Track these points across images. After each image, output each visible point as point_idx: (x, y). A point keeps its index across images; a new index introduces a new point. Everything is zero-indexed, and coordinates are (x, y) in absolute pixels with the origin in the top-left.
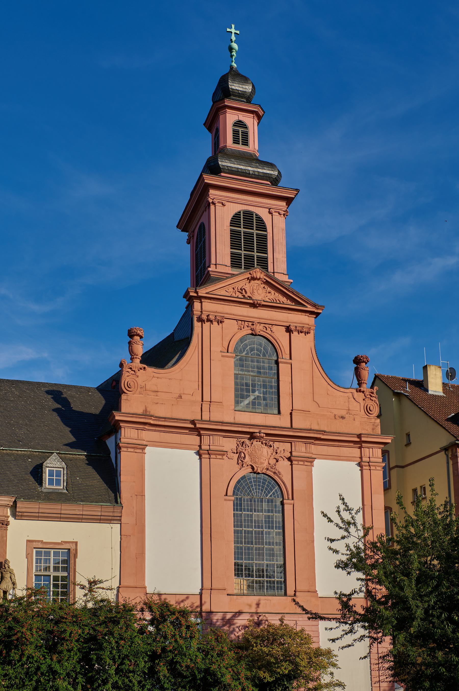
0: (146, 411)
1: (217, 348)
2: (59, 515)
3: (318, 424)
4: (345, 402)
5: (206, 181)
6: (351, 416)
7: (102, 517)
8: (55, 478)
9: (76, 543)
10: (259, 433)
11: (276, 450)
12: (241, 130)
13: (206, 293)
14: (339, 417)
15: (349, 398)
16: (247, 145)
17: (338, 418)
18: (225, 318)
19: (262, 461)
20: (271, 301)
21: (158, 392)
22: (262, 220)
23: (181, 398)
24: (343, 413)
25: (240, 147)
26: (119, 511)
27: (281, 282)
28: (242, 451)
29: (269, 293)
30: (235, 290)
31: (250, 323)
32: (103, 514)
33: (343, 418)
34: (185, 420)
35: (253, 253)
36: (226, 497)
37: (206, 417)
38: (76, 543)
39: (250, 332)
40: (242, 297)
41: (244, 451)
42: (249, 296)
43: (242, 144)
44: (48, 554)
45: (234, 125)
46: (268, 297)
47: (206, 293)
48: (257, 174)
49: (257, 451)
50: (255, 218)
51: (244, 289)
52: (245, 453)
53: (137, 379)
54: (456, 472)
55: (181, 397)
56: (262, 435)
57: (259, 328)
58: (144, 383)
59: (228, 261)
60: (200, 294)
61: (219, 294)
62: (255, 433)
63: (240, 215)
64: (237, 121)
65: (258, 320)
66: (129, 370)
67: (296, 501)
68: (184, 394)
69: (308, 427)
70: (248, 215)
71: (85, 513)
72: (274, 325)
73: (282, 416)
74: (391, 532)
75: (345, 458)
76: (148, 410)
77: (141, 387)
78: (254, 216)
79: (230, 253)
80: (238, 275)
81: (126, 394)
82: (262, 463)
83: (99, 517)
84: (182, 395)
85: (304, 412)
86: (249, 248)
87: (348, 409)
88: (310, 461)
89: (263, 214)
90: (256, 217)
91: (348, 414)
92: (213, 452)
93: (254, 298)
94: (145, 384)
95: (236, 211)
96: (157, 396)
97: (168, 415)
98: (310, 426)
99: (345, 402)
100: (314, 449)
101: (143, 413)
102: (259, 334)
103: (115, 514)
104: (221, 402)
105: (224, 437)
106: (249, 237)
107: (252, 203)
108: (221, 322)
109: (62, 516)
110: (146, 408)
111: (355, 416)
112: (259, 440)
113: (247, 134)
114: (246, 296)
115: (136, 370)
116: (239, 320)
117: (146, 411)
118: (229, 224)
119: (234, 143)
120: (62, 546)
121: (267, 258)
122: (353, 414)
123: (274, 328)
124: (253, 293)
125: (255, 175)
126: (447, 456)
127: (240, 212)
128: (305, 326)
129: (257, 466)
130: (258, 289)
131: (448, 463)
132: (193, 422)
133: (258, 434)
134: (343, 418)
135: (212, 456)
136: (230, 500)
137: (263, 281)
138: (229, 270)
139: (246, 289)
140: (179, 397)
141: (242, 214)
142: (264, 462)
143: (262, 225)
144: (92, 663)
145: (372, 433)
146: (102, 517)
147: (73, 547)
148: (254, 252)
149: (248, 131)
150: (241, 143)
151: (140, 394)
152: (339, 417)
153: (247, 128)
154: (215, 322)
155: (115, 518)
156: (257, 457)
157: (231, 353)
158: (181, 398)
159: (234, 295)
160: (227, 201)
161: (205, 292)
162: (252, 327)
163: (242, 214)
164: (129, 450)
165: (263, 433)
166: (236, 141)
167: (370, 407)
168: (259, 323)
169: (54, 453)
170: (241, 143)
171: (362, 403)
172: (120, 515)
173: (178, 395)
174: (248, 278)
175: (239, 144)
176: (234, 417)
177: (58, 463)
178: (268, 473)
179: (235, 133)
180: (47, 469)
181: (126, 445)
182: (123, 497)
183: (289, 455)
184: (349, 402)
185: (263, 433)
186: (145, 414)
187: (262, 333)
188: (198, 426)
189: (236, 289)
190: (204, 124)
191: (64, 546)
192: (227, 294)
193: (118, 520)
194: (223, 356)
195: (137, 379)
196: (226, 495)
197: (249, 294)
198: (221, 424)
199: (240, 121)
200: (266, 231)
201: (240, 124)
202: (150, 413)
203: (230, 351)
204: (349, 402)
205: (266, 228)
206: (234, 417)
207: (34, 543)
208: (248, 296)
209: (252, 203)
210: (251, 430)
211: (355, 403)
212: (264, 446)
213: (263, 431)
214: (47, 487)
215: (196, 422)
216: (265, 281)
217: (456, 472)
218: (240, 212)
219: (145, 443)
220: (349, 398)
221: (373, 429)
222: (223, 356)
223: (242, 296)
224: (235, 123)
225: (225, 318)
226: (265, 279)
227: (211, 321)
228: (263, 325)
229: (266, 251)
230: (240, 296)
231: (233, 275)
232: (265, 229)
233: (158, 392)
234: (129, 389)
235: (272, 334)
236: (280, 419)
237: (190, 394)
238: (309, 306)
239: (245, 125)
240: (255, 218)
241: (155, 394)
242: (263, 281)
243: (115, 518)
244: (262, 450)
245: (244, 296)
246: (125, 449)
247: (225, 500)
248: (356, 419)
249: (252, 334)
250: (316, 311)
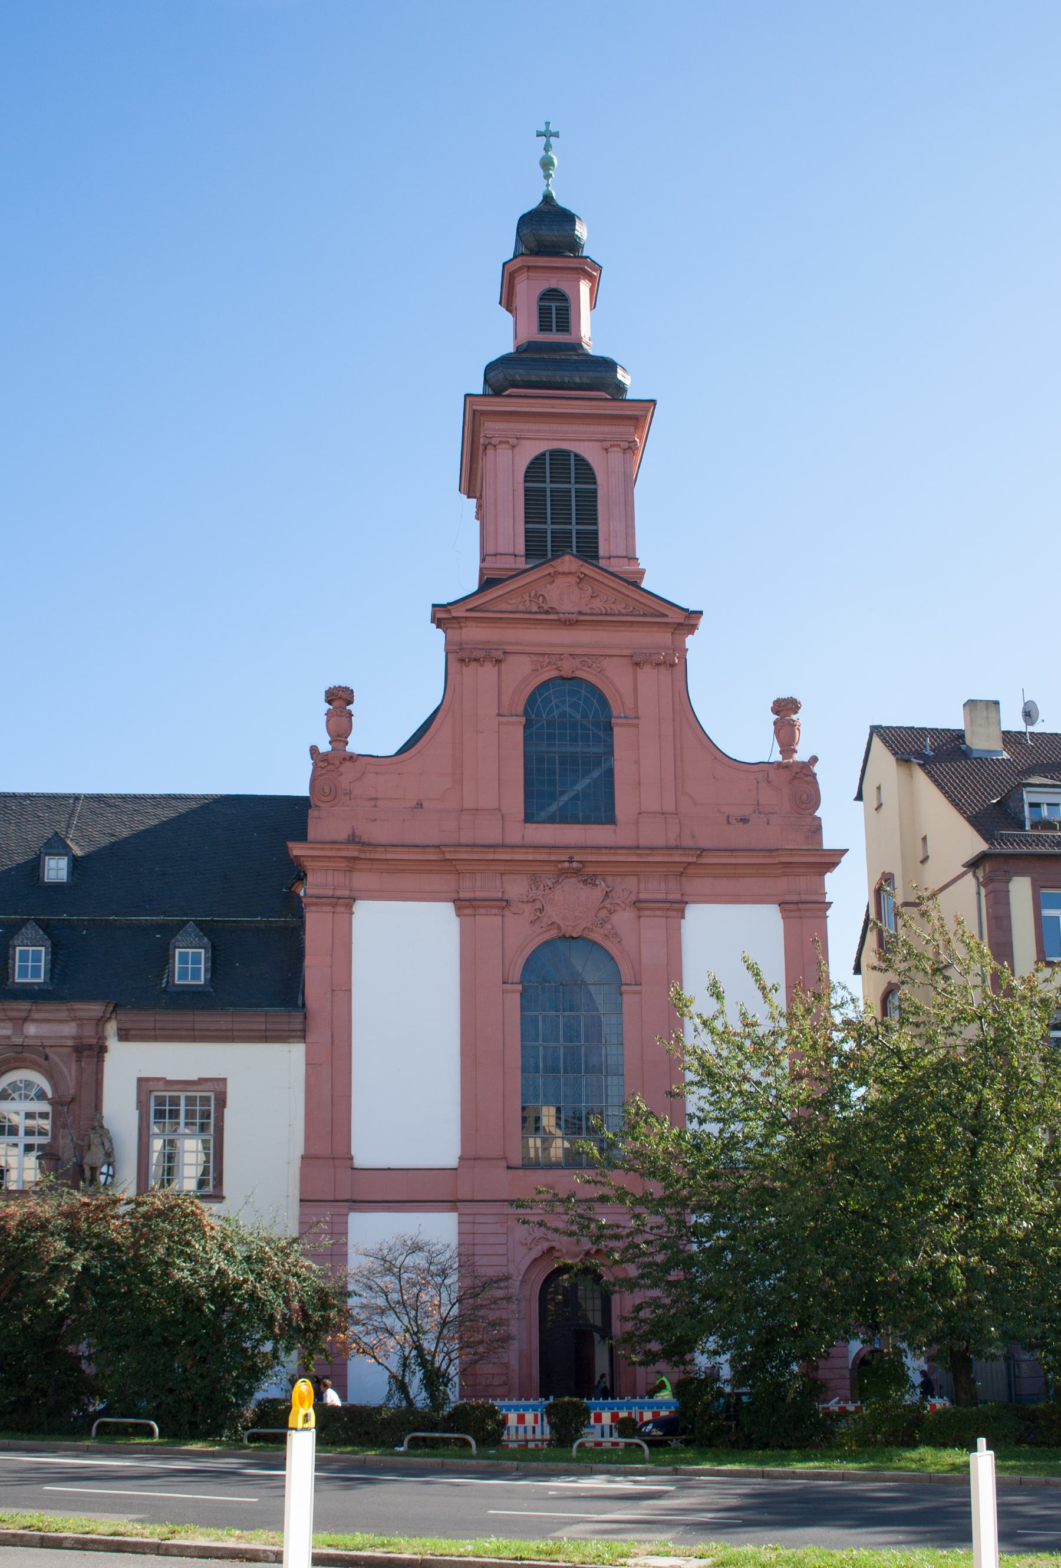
8: (190, 966)
12: (554, 305)
13: (468, 610)
17: (735, 822)
21: (377, 799)
22: (588, 464)
24: (746, 811)
32: (269, 1026)
33: (744, 820)
35: (568, 527)
43: (557, 330)
45: (541, 299)
47: (468, 610)
51: (541, 595)
74: (224, 1507)
76: (357, 833)
78: (572, 458)
90: (575, 460)
96: (375, 806)
110: (353, 830)
123: (605, 663)
126: (978, 879)
131: (979, 893)
134: (744, 820)
136: (513, 992)
139: (546, 595)
141: (548, 457)
144: (83, 1394)
150: (554, 328)
163: (548, 457)
169: (188, 921)
175: (551, 330)
193: (302, 1035)
200: (595, 483)
205: (595, 478)
207: (151, 1083)
213: (576, 858)
220: (758, 782)
221: (814, 833)
236: (615, 832)
239: (564, 296)
241: (373, 803)
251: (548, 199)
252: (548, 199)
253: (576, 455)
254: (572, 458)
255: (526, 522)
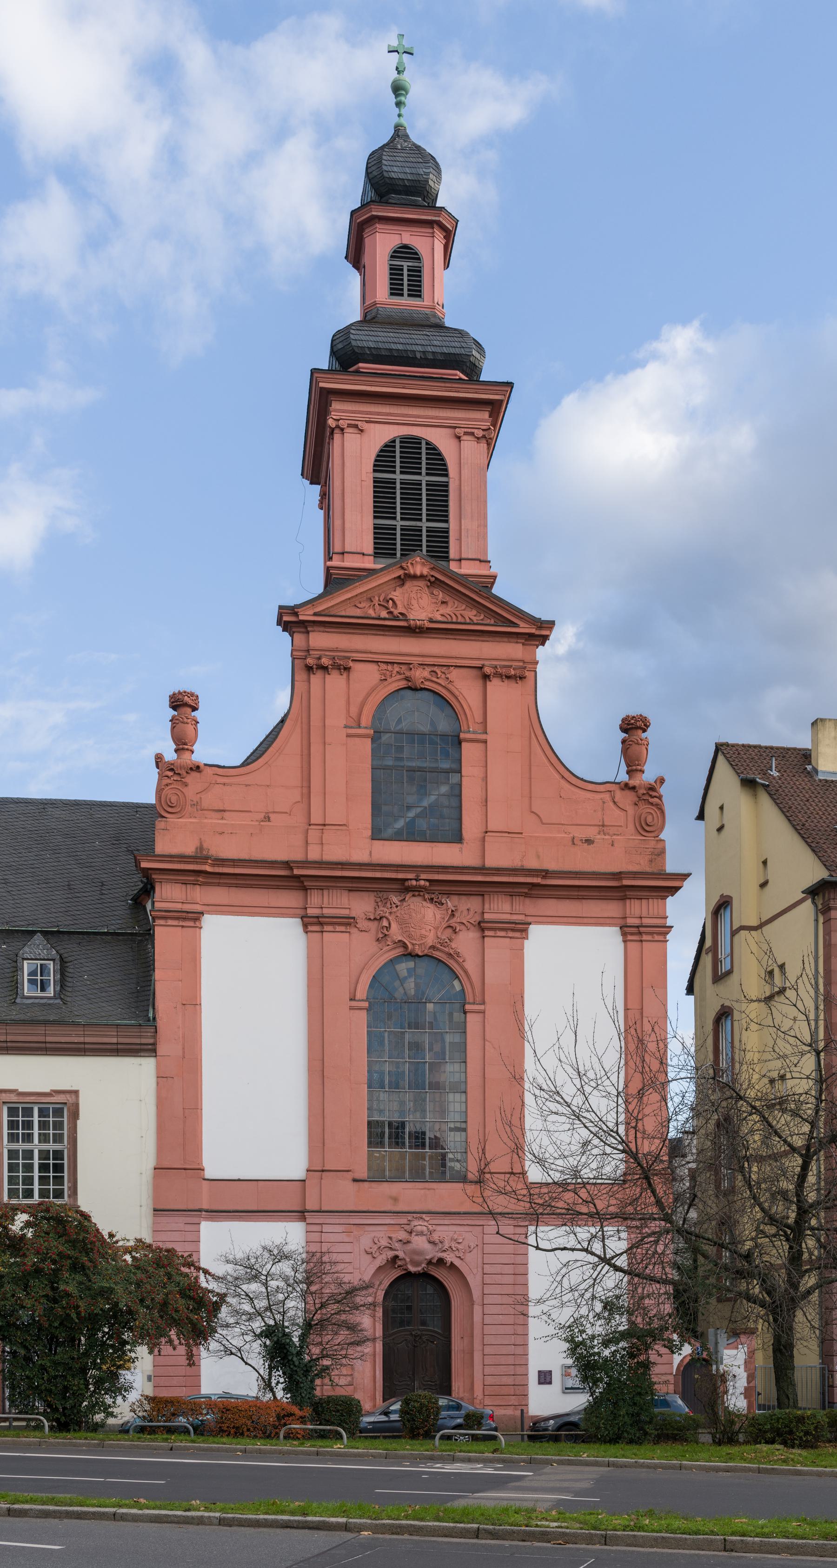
0: (201, 848)
1: (337, 720)
2: (43, 1045)
3: (538, 857)
4: (595, 811)
5: (322, 385)
6: (607, 837)
7: (119, 1047)
9: (76, 1093)
10: (416, 880)
11: (452, 911)
12: (406, 265)
13: (315, 614)
14: (582, 840)
15: (604, 802)
16: (420, 296)
17: (580, 843)
18: (353, 660)
19: (423, 932)
20: (445, 620)
21: (224, 811)
22: (440, 454)
23: (269, 821)
24: (591, 833)
25: (405, 302)
26: (149, 1034)
27: (459, 577)
28: (384, 915)
29: (443, 603)
30: (373, 604)
31: (404, 667)
33: (589, 841)
34: (272, 864)
35: (418, 524)
36: (354, 1004)
37: (314, 854)
38: (76, 1093)
39: (403, 684)
40: (390, 616)
41: (387, 915)
42: (401, 614)
43: (409, 295)
44: (28, 1112)
46: (441, 612)
47: (315, 614)
48: (430, 356)
49: (414, 915)
50: (424, 451)
51: (391, 599)
52: (390, 918)
53: (185, 790)
54: (827, 937)
55: (269, 818)
56: (422, 883)
57: (420, 675)
58: (199, 796)
59: (368, 546)
60: (301, 618)
61: (343, 613)
62: (407, 880)
63: (394, 447)
64: (399, 248)
65: (420, 660)
66: (170, 774)
67: (490, 1008)
68: (274, 812)
69: (517, 864)
70: (411, 444)
71: (88, 1040)
72: (452, 666)
73: (465, 844)
75: (593, 921)
76: (205, 846)
77: (192, 803)
78: (424, 446)
79: (372, 527)
80: (382, 570)
81: (164, 819)
82: (423, 937)
83: (115, 1047)
84: (270, 815)
85: (510, 835)
86: (411, 512)
87: (601, 823)
88: (520, 929)
89: (441, 439)
90: (427, 449)
91: (602, 833)
92: (327, 920)
93: (411, 617)
94: (201, 798)
95: (391, 437)
96: (222, 818)
97: (244, 856)
98: (521, 861)
99: (595, 811)
100: (529, 907)
101: (196, 852)
102: (423, 686)
103: (144, 1041)
104: (344, 825)
105: (350, 890)
106: (411, 491)
107: (418, 420)
108: (345, 669)
109: (48, 1045)
110: (201, 843)
111: (614, 837)
112: (417, 893)
113: (420, 271)
114: (396, 612)
115: (183, 772)
116: (381, 662)
117: (201, 848)
118: (371, 468)
119: (392, 294)
120: (52, 1098)
121: (447, 531)
122: (611, 833)
123: (454, 674)
124: (409, 606)
125: (426, 359)
126: (816, 905)
127: (394, 441)
128: (486, 663)
129: (414, 942)
130: (419, 596)
131: (817, 920)
132: (287, 865)
133: (414, 883)
134: (589, 841)
135: (487, 933)
136: (361, 1009)
137: (429, 581)
138: (369, 563)
139: (395, 598)
140: (265, 818)
141: (398, 444)
142: (427, 934)
143: (438, 463)
145: (648, 870)
146: (119, 1047)
147: (70, 1099)
148: (420, 520)
149: (421, 265)
150: (406, 292)
151: (191, 817)
152: (582, 840)
153: (419, 259)
154: (334, 669)
155: (146, 1047)
156: (413, 925)
157: (366, 728)
158: (269, 821)
159: (371, 612)
160: (367, 422)
161: (311, 612)
162: (408, 674)
163: (398, 444)
164: (170, 922)
165: (424, 880)
166: (396, 290)
167: (646, 818)
168: (422, 664)
170: (406, 292)
171: (631, 810)
172: (151, 1041)
173: (262, 815)
174: (399, 577)
175: (402, 295)
176: (371, 852)
177: (45, 951)
178: (437, 954)
179: (395, 273)
180: (25, 962)
181: (164, 914)
182: (160, 1008)
183: (478, 918)
184: (603, 810)
185: (424, 880)
186: (200, 856)
187: (428, 685)
188: (296, 872)
189: (376, 601)
190: (346, 258)
191: (55, 1098)
192: (358, 612)
193: (150, 1050)
194: (348, 736)
195: (185, 790)
196: (352, 999)
197: (401, 609)
198: (340, 867)
199: (405, 247)
200: (447, 475)
201: (404, 252)
202: (208, 852)
203: (363, 724)
204: (603, 810)
205: (446, 470)
206: (371, 852)
208: (399, 613)
209: (418, 420)
210: (400, 876)
211: (618, 812)
212: (429, 905)
213: (423, 876)
214: (25, 994)
215: (292, 865)
216: (433, 579)
217: (827, 937)
218: (394, 441)
219: (198, 908)
220: (604, 802)
222: (348, 736)
223: (388, 613)
224: (395, 252)
225: (353, 660)
226: (432, 576)
227: (324, 668)
228: (429, 669)
229: (447, 516)
230: (384, 614)
231: (371, 572)
232: (445, 472)
233: (224, 811)
234: (170, 810)
235: (450, 686)
236: (461, 850)
237: (286, 813)
238: (522, 624)
239: (416, 254)
240: (424, 451)
241: (219, 815)
242: (429, 581)
243: (146, 1047)
244: (423, 912)
245: (390, 613)
246: (162, 922)
247: (351, 1008)
248: (616, 844)
249: (409, 688)
250: (538, 632)
251: (399, 132)
252: (399, 132)
253: (428, 443)
254: (424, 446)
255: (375, 517)
